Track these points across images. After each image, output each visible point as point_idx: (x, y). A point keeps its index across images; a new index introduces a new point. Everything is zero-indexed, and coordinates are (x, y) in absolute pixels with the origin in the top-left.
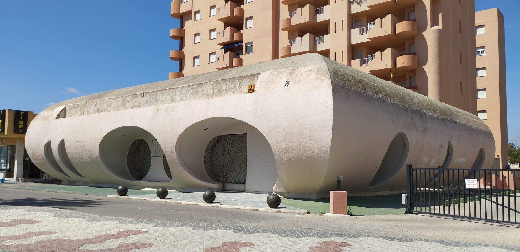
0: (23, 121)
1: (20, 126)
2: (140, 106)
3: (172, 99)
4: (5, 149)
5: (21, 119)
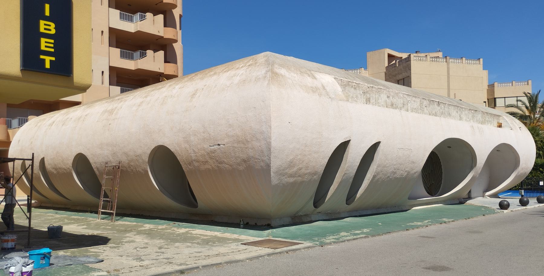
0: (53, 25)
1: (43, 40)
2: (436, 115)
3: (460, 117)
4: (540, 195)
5: (47, 13)
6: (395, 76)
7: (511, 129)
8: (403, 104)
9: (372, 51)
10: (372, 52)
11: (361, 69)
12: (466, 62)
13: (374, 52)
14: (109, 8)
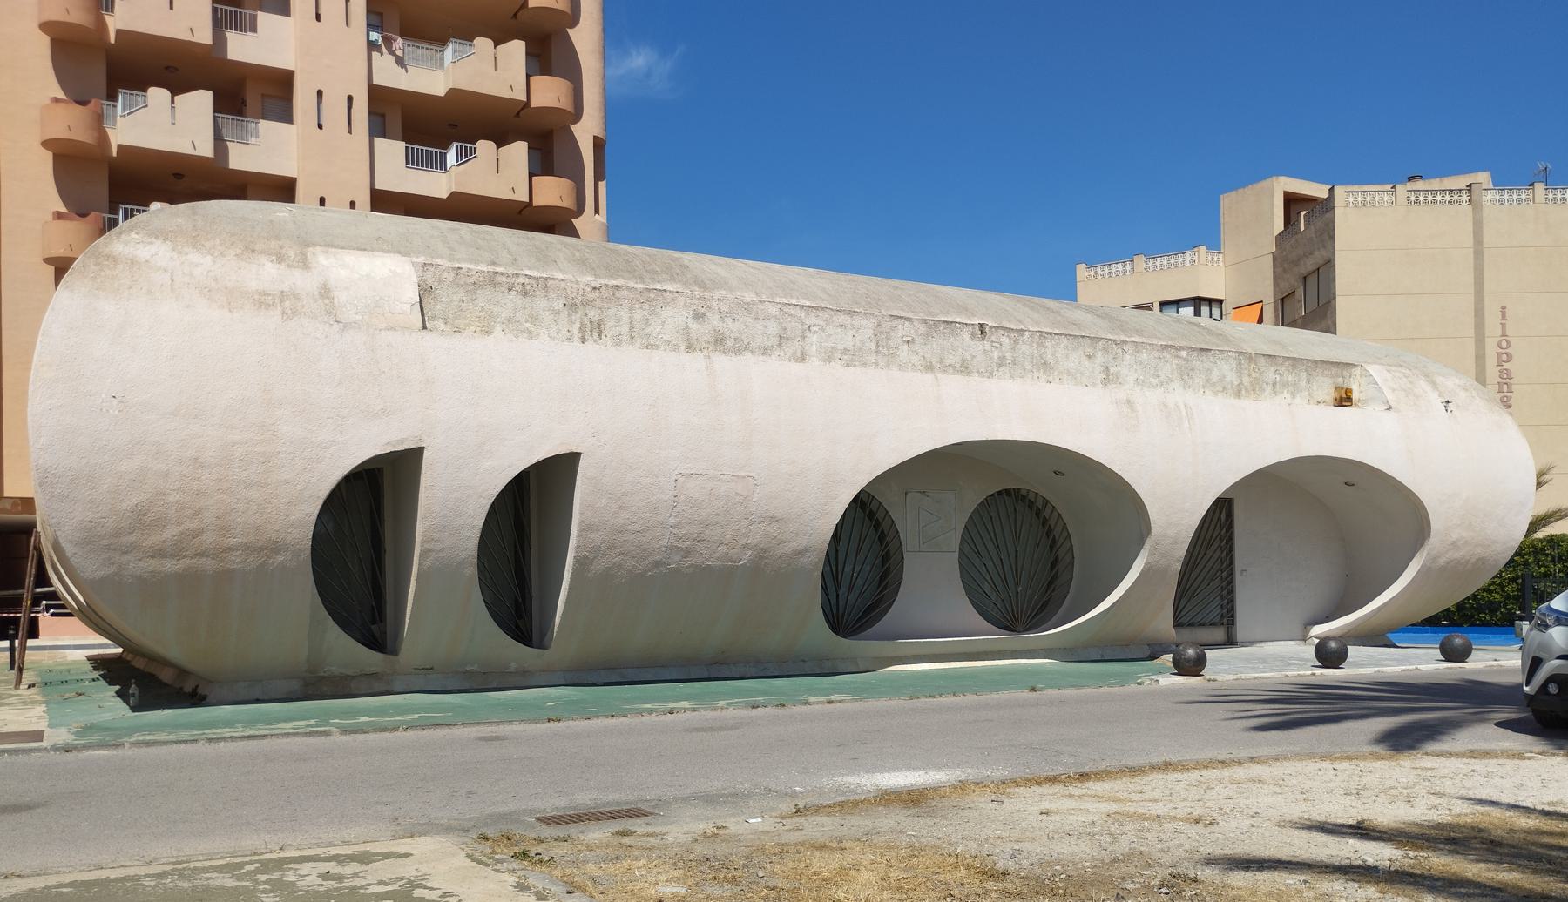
3: (1108, 375)
6: (1296, 263)
7: (1389, 409)
8: (780, 337)
9: (1236, 188)
10: (1234, 192)
11: (1196, 249)
12: (1551, 196)
13: (1241, 191)
14: (377, 141)
